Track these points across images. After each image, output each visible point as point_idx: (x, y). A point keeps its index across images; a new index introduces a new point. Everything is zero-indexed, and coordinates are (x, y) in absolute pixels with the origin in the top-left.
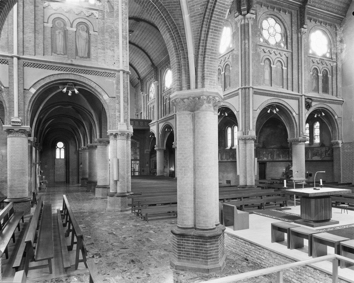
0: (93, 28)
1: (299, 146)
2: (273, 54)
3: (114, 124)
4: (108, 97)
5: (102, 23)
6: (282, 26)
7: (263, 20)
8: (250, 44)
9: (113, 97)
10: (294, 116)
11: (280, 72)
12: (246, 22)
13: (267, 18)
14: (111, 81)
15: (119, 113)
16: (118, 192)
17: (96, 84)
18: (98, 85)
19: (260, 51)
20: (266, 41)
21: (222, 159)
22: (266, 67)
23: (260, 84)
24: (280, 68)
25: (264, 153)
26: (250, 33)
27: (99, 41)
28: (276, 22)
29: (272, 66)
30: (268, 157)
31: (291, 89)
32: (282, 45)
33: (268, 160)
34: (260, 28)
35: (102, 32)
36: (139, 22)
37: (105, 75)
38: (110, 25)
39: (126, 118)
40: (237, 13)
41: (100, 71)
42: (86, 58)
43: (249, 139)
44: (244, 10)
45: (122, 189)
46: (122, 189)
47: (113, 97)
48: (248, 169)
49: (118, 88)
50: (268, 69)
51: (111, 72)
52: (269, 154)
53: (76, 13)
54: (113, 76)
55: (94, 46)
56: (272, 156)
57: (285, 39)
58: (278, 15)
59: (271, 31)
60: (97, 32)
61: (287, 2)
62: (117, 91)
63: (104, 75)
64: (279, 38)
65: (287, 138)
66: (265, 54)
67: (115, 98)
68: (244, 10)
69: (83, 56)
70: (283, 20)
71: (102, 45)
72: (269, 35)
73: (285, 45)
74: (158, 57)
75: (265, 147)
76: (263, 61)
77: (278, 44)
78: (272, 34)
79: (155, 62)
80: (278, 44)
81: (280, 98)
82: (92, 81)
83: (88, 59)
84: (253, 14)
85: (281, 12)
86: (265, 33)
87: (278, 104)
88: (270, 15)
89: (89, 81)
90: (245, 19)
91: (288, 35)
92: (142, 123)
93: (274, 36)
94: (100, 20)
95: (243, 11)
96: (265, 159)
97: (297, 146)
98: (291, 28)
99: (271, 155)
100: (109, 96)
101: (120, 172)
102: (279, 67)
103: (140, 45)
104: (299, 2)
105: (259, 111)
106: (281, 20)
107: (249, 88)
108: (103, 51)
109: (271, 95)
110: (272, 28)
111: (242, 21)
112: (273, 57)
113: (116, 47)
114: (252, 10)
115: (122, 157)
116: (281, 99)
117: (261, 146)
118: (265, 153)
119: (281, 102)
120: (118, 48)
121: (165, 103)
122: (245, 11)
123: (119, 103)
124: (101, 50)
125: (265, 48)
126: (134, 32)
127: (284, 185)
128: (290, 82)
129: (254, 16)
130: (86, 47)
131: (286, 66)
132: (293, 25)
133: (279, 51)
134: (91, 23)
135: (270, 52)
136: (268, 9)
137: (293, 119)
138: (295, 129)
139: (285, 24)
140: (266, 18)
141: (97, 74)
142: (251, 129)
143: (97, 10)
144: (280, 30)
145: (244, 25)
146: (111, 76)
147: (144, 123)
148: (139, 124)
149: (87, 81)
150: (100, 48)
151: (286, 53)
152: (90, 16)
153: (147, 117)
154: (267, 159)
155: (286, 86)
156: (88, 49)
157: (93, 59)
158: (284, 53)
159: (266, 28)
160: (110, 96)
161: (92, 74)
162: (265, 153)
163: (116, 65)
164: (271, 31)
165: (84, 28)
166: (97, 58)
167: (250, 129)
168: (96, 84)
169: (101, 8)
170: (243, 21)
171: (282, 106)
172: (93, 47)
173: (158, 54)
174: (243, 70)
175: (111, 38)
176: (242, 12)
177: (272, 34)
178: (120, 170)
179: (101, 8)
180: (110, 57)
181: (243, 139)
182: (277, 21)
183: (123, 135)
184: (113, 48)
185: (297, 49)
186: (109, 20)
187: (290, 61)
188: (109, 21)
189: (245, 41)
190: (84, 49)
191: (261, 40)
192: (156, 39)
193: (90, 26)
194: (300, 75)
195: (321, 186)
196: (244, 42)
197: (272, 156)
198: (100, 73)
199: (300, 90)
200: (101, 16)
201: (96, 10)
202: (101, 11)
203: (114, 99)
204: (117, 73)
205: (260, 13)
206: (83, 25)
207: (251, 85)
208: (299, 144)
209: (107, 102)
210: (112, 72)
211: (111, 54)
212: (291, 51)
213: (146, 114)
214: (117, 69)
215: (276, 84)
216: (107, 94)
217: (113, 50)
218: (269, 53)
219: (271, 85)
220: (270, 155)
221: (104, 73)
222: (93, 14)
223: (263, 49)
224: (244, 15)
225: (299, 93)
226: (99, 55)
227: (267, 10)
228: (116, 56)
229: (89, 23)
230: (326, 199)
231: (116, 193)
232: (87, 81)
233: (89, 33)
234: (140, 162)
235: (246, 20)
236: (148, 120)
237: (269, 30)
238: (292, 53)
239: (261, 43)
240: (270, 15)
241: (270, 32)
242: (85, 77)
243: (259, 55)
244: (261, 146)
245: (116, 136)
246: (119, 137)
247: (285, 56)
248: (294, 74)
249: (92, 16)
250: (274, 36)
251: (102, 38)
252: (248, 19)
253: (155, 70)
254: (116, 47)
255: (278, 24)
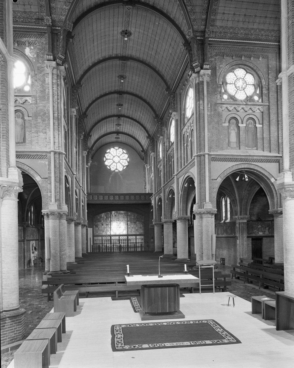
0: (28, 113)
1: (280, 218)
2: (242, 110)
3: (47, 204)
4: (40, 179)
5: (35, 108)
6: (255, 75)
7: (228, 73)
8: (205, 105)
9: (45, 178)
10: (272, 182)
11: (253, 132)
12: (201, 79)
13: (234, 69)
14: (43, 162)
15: (50, 193)
16: (50, 271)
17: (29, 167)
18: (30, 168)
19: (222, 110)
20: (232, 98)
21: (218, 234)
22: (232, 127)
23: (222, 149)
24: (253, 126)
25: (259, 227)
26: (204, 92)
27: (33, 126)
28: (247, 72)
29: (240, 125)
30: (265, 231)
31: (269, 150)
32: (256, 98)
33: (265, 235)
34: (221, 83)
35: (36, 116)
36: (122, 95)
37: (37, 158)
38: (43, 108)
39: (58, 198)
40: (190, 72)
41: (32, 154)
42: (22, 143)
43: (204, 213)
44: (197, 66)
45: (53, 268)
46: (53, 268)
47: (45, 178)
48: (204, 247)
49: (49, 169)
50: (235, 130)
51: (43, 154)
52: (266, 228)
53: (21, 103)
54: (45, 158)
55: (28, 131)
56: (271, 230)
57: (259, 90)
58: (247, 63)
59: (240, 84)
60: (31, 117)
61: (259, 46)
62: (49, 171)
63: (36, 157)
64: (250, 90)
65: (269, 209)
66: (230, 113)
67: (47, 178)
68: (197, 66)
69: (19, 141)
70: (255, 68)
71: (36, 129)
72: (236, 90)
73: (259, 98)
74: (151, 127)
75: (260, 219)
76: (227, 121)
77: (249, 99)
78: (240, 87)
79: (151, 133)
80: (248, 99)
81: (251, 163)
82: (25, 164)
83: (24, 144)
84: (208, 69)
85: (252, 59)
86: (231, 89)
87: (247, 170)
88: (236, 65)
89: (22, 165)
90: (199, 77)
91: (263, 85)
92: (142, 197)
93: (244, 90)
94: (33, 105)
95: (196, 68)
96: (261, 234)
97: (278, 218)
98: (267, 76)
99: (269, 229)
100: (41, 177)
101: (51, 251)
102: (250, 126)
103: (135, 117)
104: (276, 43)
105: (220, 181)
106: (252, 69)
107: (204, 156)
108: (36, 135)
109: (236, 160)
110: (241, 80)
111: (196, 79)
112: (242, 114)
113: (47, 129)
114: (206, 65)
115: (53, 237)
116: (253, 163)
117: (254, 218)
118: (260, 226)
119: (252, 167)
120: (50, 130)
121: (160, 175)
122: (198, 67)
123: (50, 184)
124: (35, 134)
125: (228, 106)
126: (124, 105)
127: (184, 270)
128: (266, 141)
129: (209, 72)
130: (22, 134)
131: (261, 122)
132: (269, 72)
133: (249, 107)
134: (25, 109)
135: (236, 110)
136: (233, 59)
137: (272, 187)
138: (275, 198)
139: (258, 73)
140: (232, 70)
141: (29, 157)
142: (207, 201)
143: (30, 96)
144: (253, 81)
145: (198, 83)
146: (43, 158)
147: (145, 197)
148: (145, 199)
149: (20, 164)
150: (34, 132)
151: (260, 107)
152: (25, 103)
153: (150, 190)
154: (263, 234)
155: (262, 147)
156: (23, 134)
157: (28, 143)
158: (258, 107)
159: (232, 82)
160: (42, 177)
161: (25, 157)
162: (260, 226)
163: (48, 147)
164: (240, 84)
165: (20, 115)
166: (31, 142)
167: (206, 202)
168: (29, 167)
169: (34, 93)
170: (197, 79)
171: (255, 172)
172: (28, 132)
173: (151, 124)
174: (198, 135)
175: (44, 121)
176: (195, 69)
177: (240, 87)
178: (51, 249)
179: (34, 93)
180: (42, 139)
181: (198, 214)
182: (248, 71)
183: (53, 215)
184: (45, 131)
185: (276, 100)
186: (41, 103)
187: (266, 116)
188: (41, 105)
189: (200, 103)
190: (20, 135)
191: (225, 97)
192: (139, 109)
193: (24, 112)
194: (280, 132)
195: (186, 272)
196: (198, 103)
197: (271, 230)
198: (33, 156)
199: (281, 150)
200: (34, 102)
201: (29, 96)
202: (34, 96)
203: (46, 180)
204: (48, 155)
205: (221, 66)
206: (19, 113)
207: (207, 151)
208: (280, 216)
209: (40, 183)
210: (44, 154)
211: (44, 137)
212: (268, 104)
213: (150, 187)
214: (48, 150)
215: (247, 146)
216: (39, 175)
217: (46, 132)
218: (235, 110)
219: (240, 148)
220: (267, 228)
221: (36, 155)
222: (27, 100)
223: (226, 108)
224: (198, 72)
225: (279, 154)
226: (33, 139)
227: (231, 60)
228: (47, 138)
229: (23, 110)
230: (164, 288)
231: (49, 271)
232: (20, 164)
233: (24, 119)
234: (145, 237)
235: (200, 77)
236: (149, 193)
237: (236, 83)
238: (269, 106)
239: (223, 100)
240: (236, 65)
241: (237, 85)
242: (18, 162)
243: (219, 115)
244: (254, 218)
245: (48, 215)
246: (50, 217)
247: (260, 112)
248: (271, 131)
249: (27, 103)
250: (244, 90)
251: (35, 122)
252: (202, 76)
253: (151, 141)
254: (47, 129)
255: (250, 73)
